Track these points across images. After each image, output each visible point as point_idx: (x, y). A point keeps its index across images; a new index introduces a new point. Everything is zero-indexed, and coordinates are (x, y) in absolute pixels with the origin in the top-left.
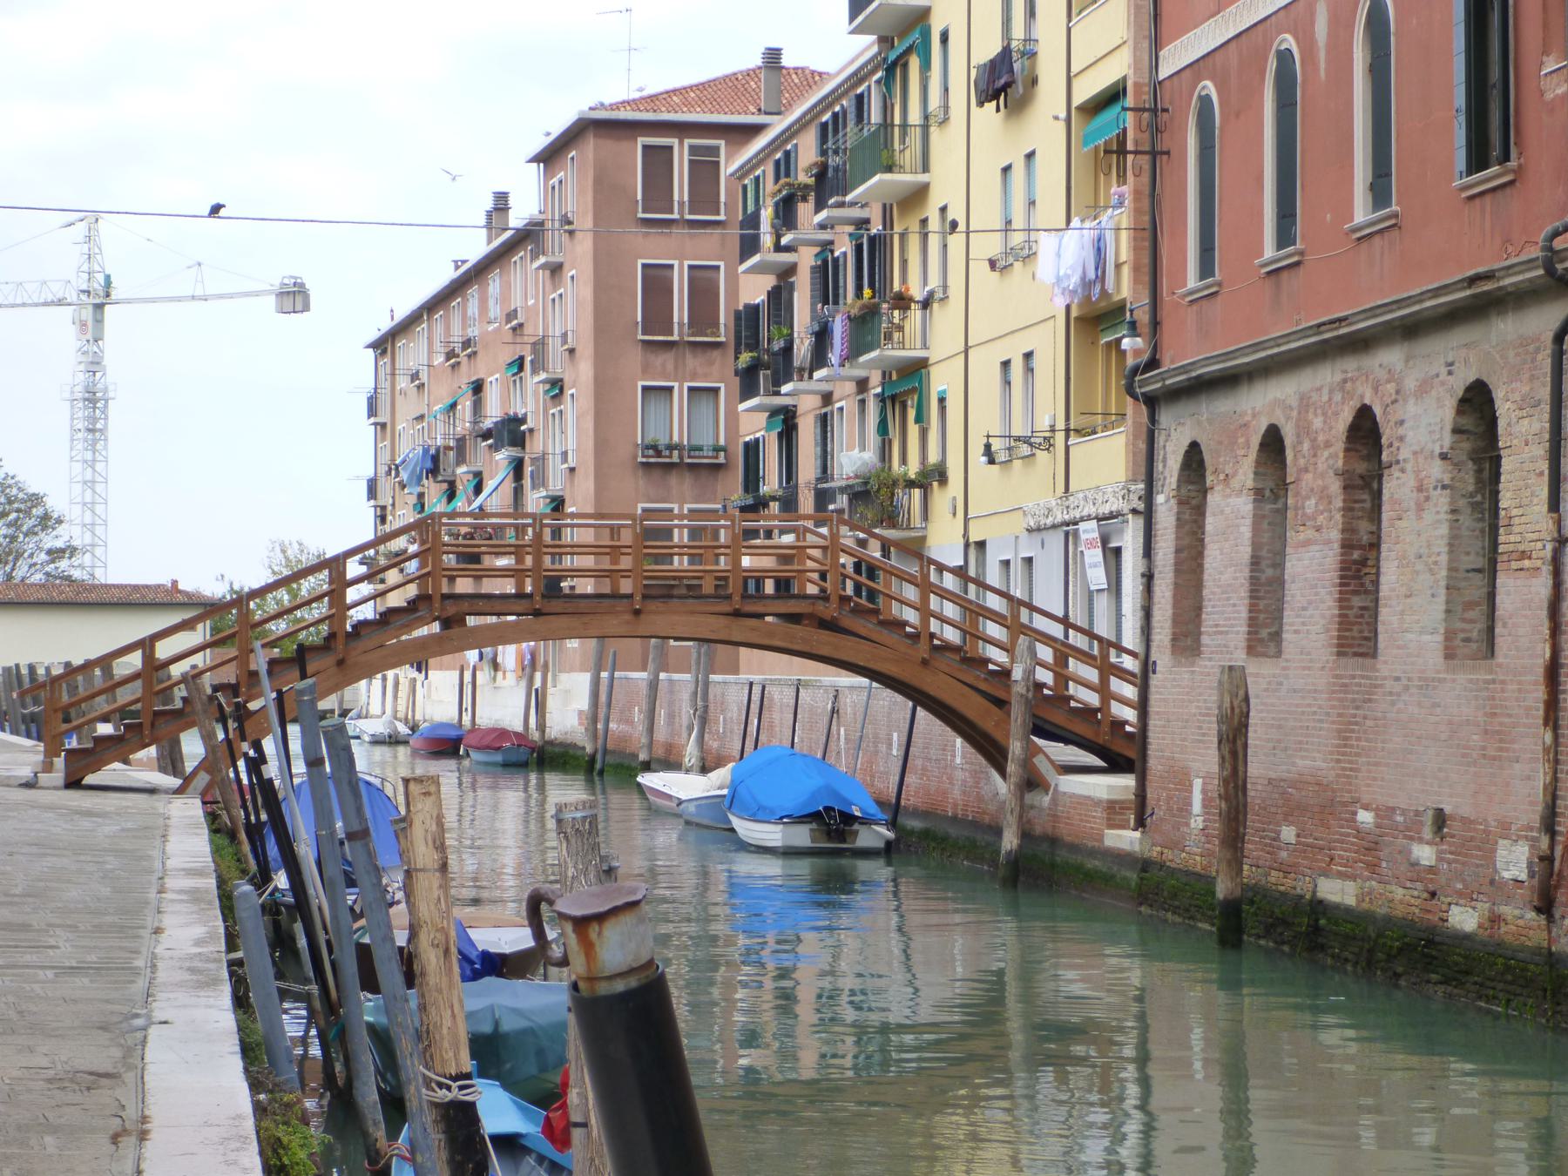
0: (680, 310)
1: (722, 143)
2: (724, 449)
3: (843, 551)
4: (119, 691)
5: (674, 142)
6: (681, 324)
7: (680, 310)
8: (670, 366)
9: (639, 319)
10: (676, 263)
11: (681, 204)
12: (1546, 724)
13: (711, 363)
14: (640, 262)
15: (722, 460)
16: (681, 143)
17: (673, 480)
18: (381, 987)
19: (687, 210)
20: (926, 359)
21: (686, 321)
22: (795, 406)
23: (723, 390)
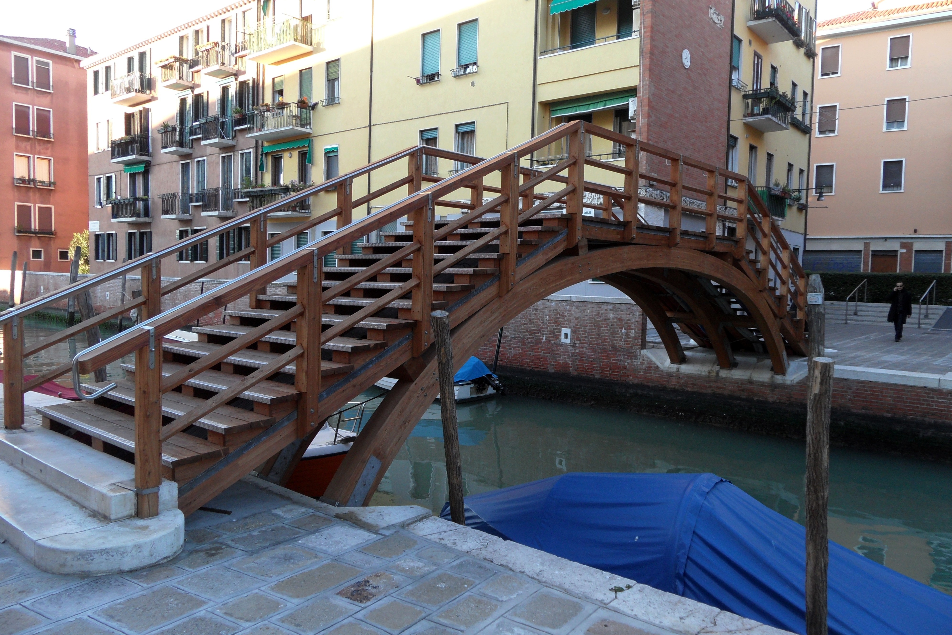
0: (33, 125)
1: (50, 62)
2: (54, 183)
3: (587, 189)
4: (374, 203)
5: (29, 57)
6: (33, 131)
7: (33, 125)
8: (29, 148)
9: (14, 126)
10: (31, 106)
11: (33, 82)
12: (890, 319)
13: (47, 149)
14: (14, 103)
15: (52, 188)
16: (32, 58)
17: (31, 194)
18: (135, 414)
19: (35, 85)
20: (310, 134)
21: (36, 130)
22: (150, 161)
23: (52, 160)
